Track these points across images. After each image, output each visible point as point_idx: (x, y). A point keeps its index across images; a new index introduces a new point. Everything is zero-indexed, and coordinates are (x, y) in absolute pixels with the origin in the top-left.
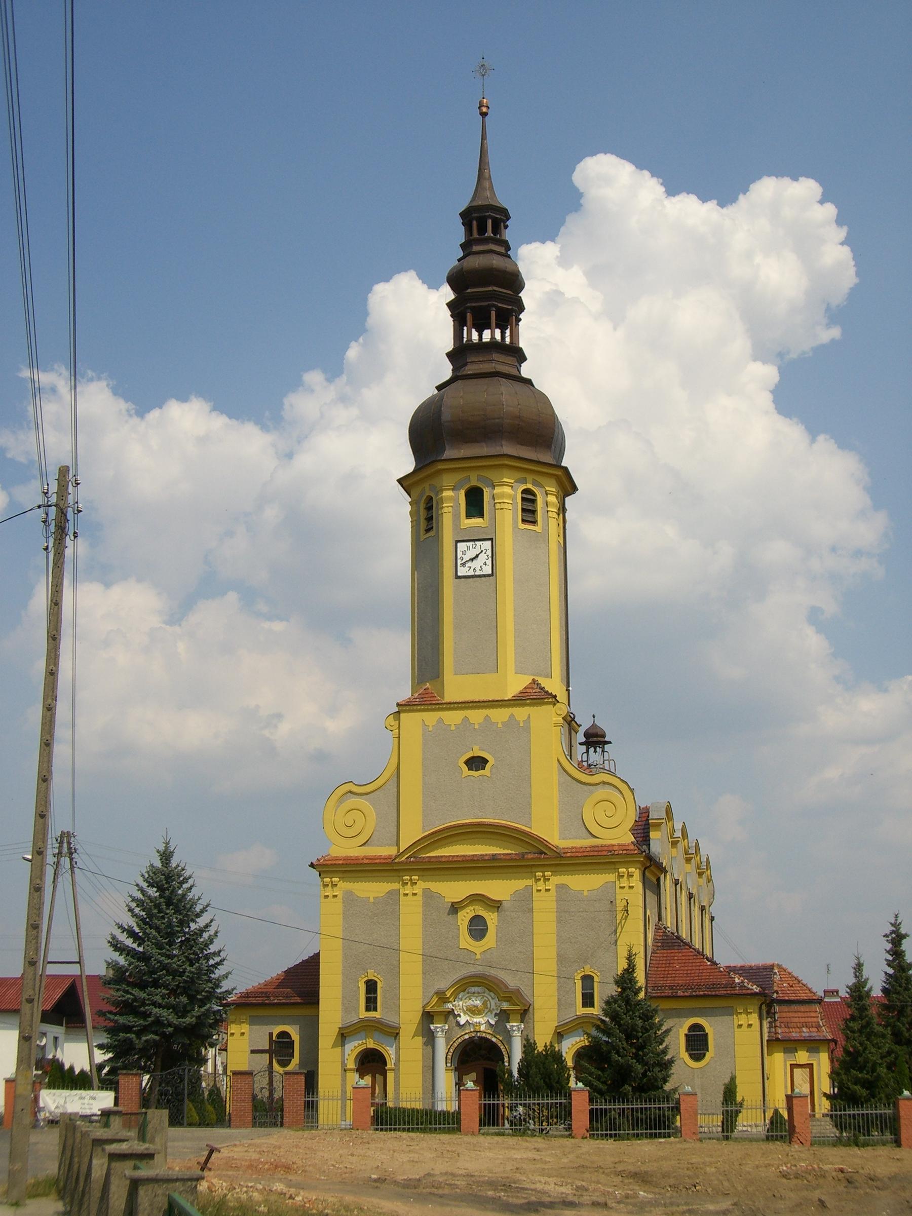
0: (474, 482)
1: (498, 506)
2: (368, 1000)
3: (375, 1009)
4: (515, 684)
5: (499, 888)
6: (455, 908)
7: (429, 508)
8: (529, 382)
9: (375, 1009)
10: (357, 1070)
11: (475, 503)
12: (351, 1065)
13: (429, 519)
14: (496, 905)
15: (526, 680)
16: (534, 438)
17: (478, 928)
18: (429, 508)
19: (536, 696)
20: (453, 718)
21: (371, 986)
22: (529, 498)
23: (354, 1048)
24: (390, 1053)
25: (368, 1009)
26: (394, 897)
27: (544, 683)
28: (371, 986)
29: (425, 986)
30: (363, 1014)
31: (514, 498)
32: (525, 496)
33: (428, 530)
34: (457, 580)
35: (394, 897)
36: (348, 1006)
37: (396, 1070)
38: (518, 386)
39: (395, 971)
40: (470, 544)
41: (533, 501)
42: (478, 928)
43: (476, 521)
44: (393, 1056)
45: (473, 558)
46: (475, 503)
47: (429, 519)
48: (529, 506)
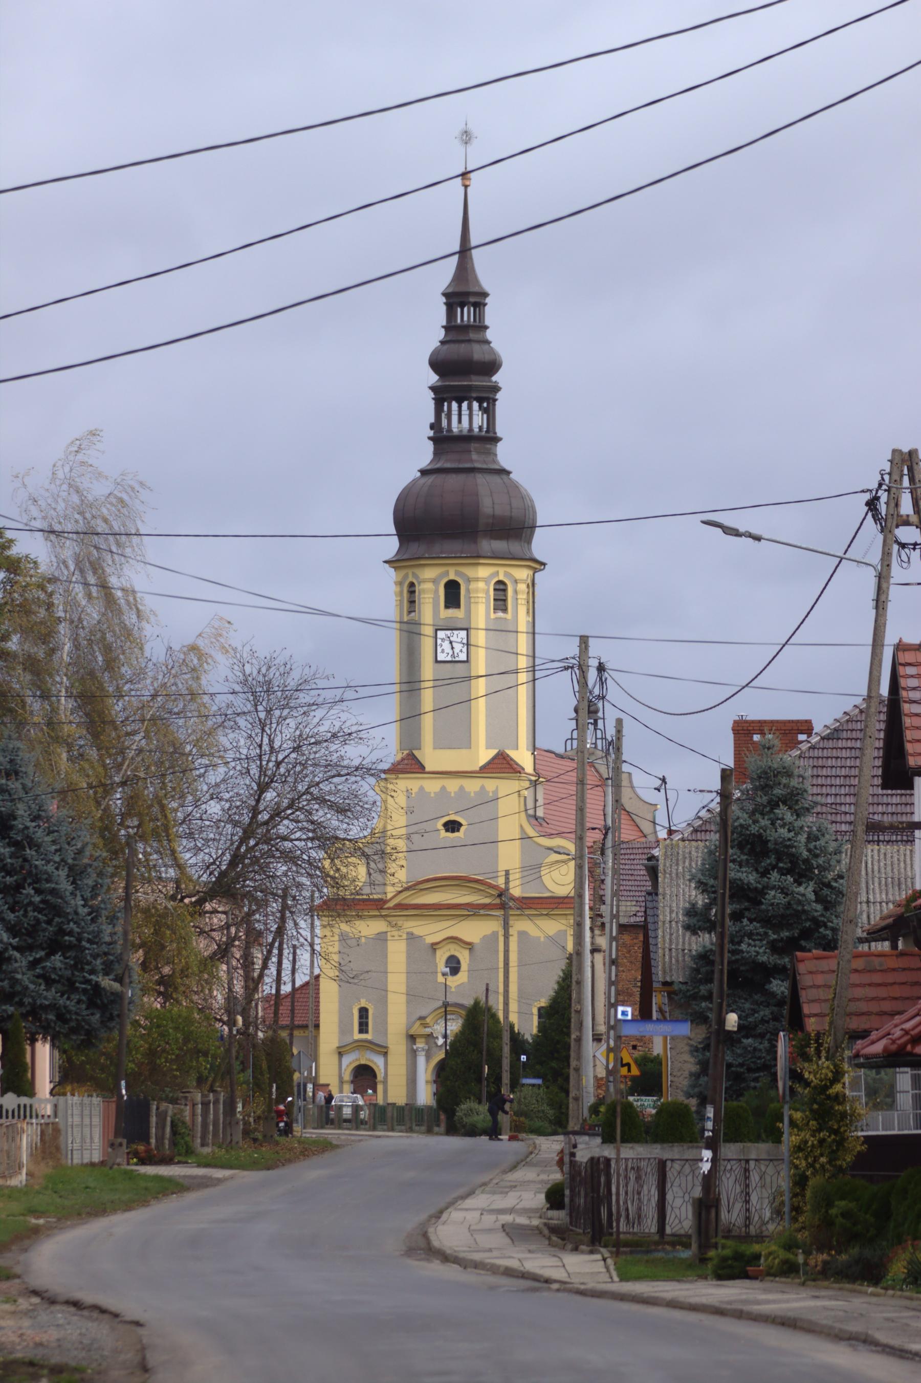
0: (452, 576)
1: (472, 600)
2: (361, 1024)
3: (367, 1032)
4: (485, 755)
5: (475, 930)
6: (434, 947)
7: (412, 592)
8: (505, 472)
9: (367, 1032)
10: (352, 1082)
11: (452, 594)
12: (347, 1076)
13: (412, 602)
14: (470, 946)
15: (492, 753)
16: (508, 530)
17: (454, 966)
18: (412, 592)
19: (501, 765)
20: (432, 786)
21: (363, 1012)
22: (501, 587)
23: (350, 1061)
24: (377, 1062)
25: (361, 1031)
26: (382, 938)
27: (512, 754)
28: (363, 1012)
29: (409, 1014)
30: (357, 1036)
31: (487, 592)
32: (498, 587)
33: (410, 612)
34: (437, 665)
35: (382, 938)
36: (344, 1029)
37: (385, 1082)
38: (496, 479)
39: (383, 1001)
40: (439, 650)
41: (505, 590)
42: (454, 966)
43: (452, 612)
44: (383, 1071)
45: (451, 646)
46: (452, 594)
47: (412, 602)
48: (501, 595)
